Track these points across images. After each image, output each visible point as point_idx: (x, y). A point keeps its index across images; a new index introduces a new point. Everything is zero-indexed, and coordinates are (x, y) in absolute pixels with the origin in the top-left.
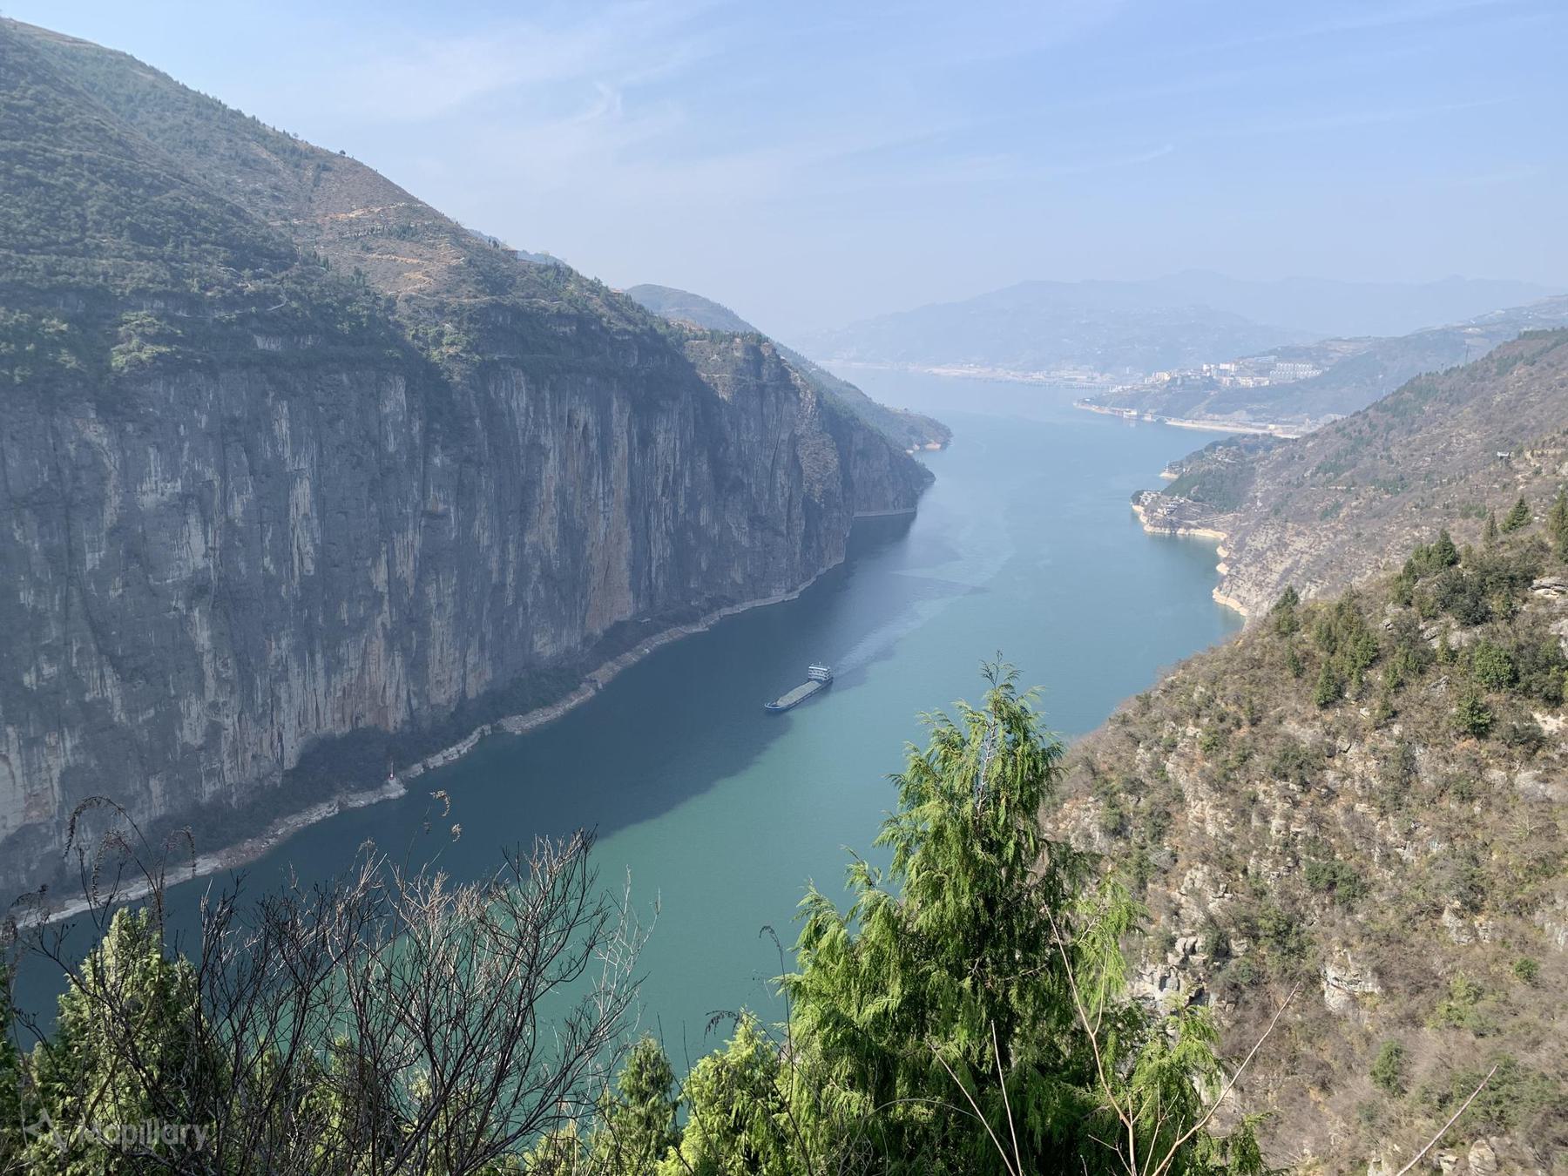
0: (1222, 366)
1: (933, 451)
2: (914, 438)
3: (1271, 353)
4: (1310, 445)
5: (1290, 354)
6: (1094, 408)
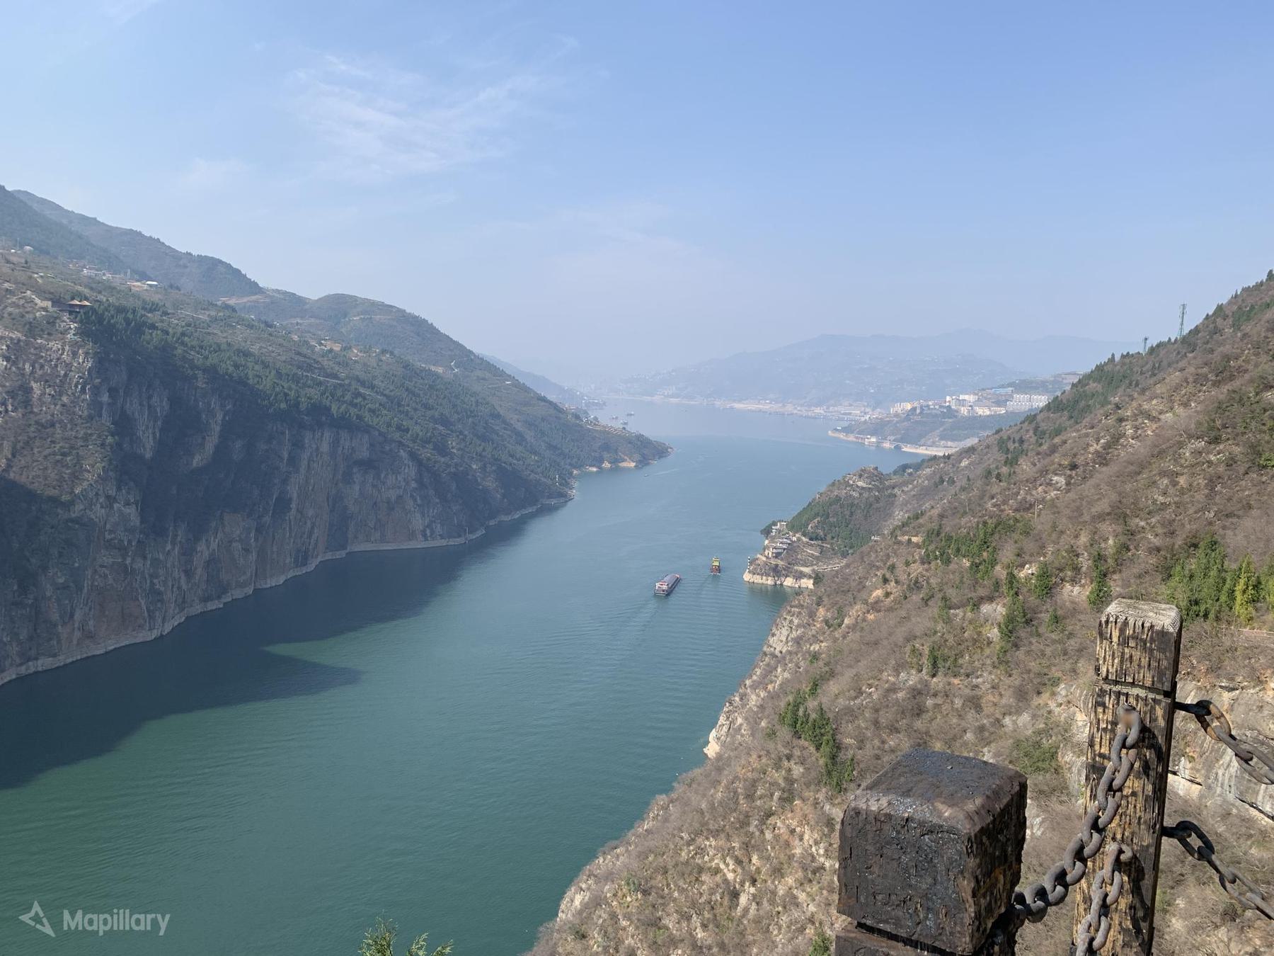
0: (962, 397)
1: (629, 469)
2: (606, 455)
3: (1010, 385)
4: (964, 463)
5: (1025, 386)
6: (842, 436)
